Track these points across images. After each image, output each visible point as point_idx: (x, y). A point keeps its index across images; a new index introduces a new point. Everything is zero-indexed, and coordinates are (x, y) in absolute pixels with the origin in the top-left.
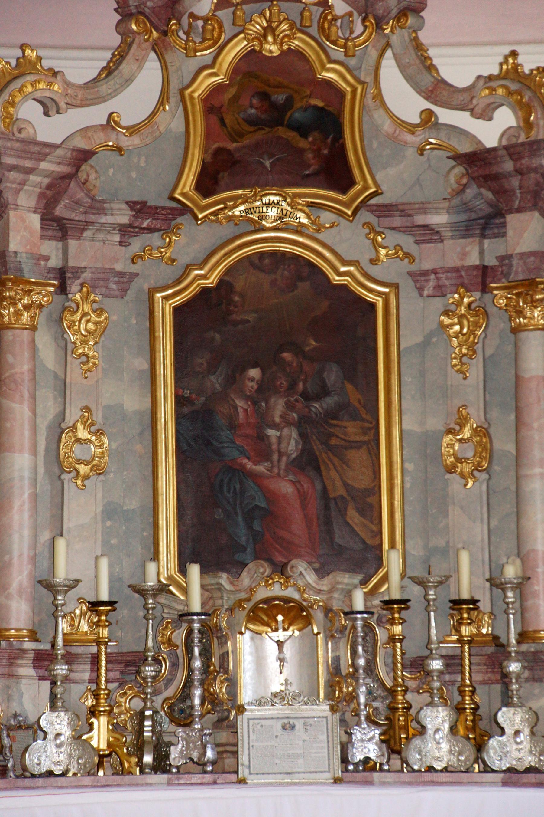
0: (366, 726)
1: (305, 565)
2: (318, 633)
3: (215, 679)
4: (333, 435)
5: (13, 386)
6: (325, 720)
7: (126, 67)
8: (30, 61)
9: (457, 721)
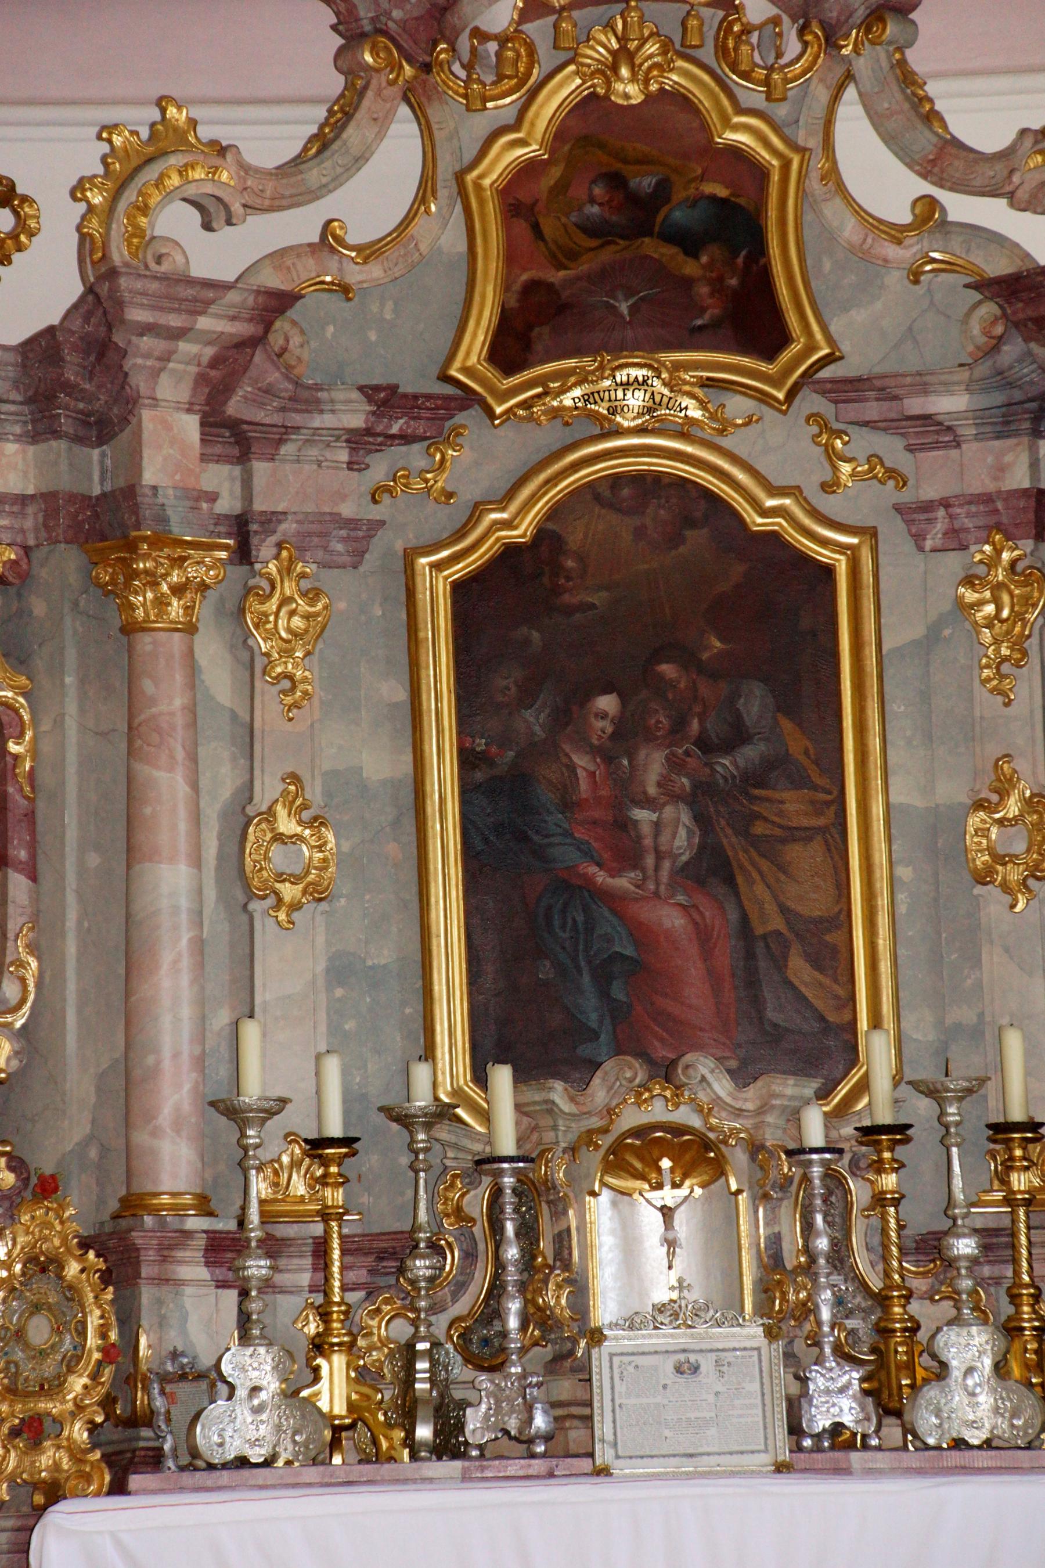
0: (834, 1364)
1: (711, 1063)
2: (739, 1192)
3: (546, 1282)
4: (757, 816)
5: (155, 738)
6: (755, 1353)
7: (351, 133)
8: (176, 129)
9: (1008, 1352)
